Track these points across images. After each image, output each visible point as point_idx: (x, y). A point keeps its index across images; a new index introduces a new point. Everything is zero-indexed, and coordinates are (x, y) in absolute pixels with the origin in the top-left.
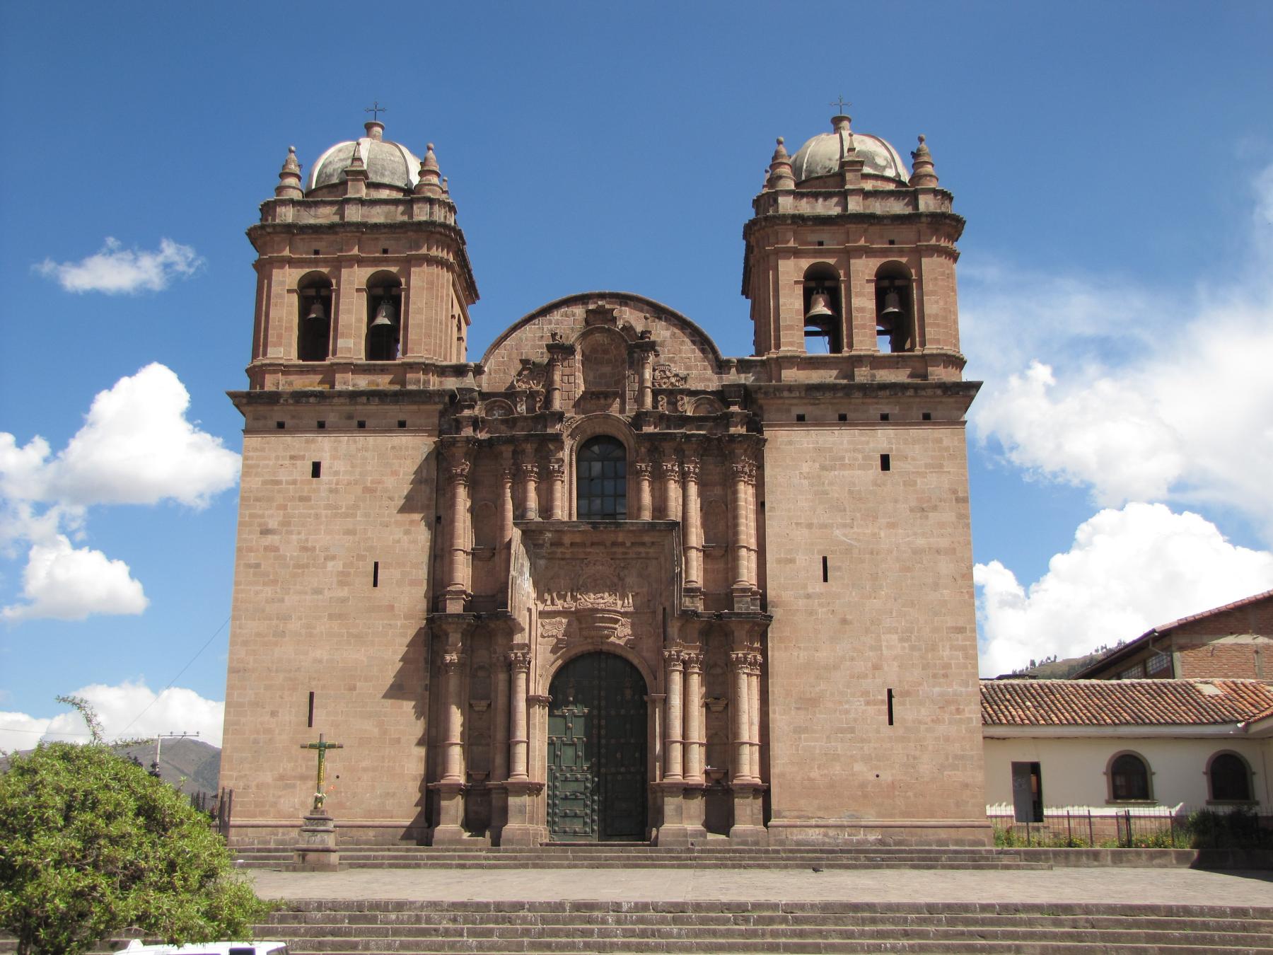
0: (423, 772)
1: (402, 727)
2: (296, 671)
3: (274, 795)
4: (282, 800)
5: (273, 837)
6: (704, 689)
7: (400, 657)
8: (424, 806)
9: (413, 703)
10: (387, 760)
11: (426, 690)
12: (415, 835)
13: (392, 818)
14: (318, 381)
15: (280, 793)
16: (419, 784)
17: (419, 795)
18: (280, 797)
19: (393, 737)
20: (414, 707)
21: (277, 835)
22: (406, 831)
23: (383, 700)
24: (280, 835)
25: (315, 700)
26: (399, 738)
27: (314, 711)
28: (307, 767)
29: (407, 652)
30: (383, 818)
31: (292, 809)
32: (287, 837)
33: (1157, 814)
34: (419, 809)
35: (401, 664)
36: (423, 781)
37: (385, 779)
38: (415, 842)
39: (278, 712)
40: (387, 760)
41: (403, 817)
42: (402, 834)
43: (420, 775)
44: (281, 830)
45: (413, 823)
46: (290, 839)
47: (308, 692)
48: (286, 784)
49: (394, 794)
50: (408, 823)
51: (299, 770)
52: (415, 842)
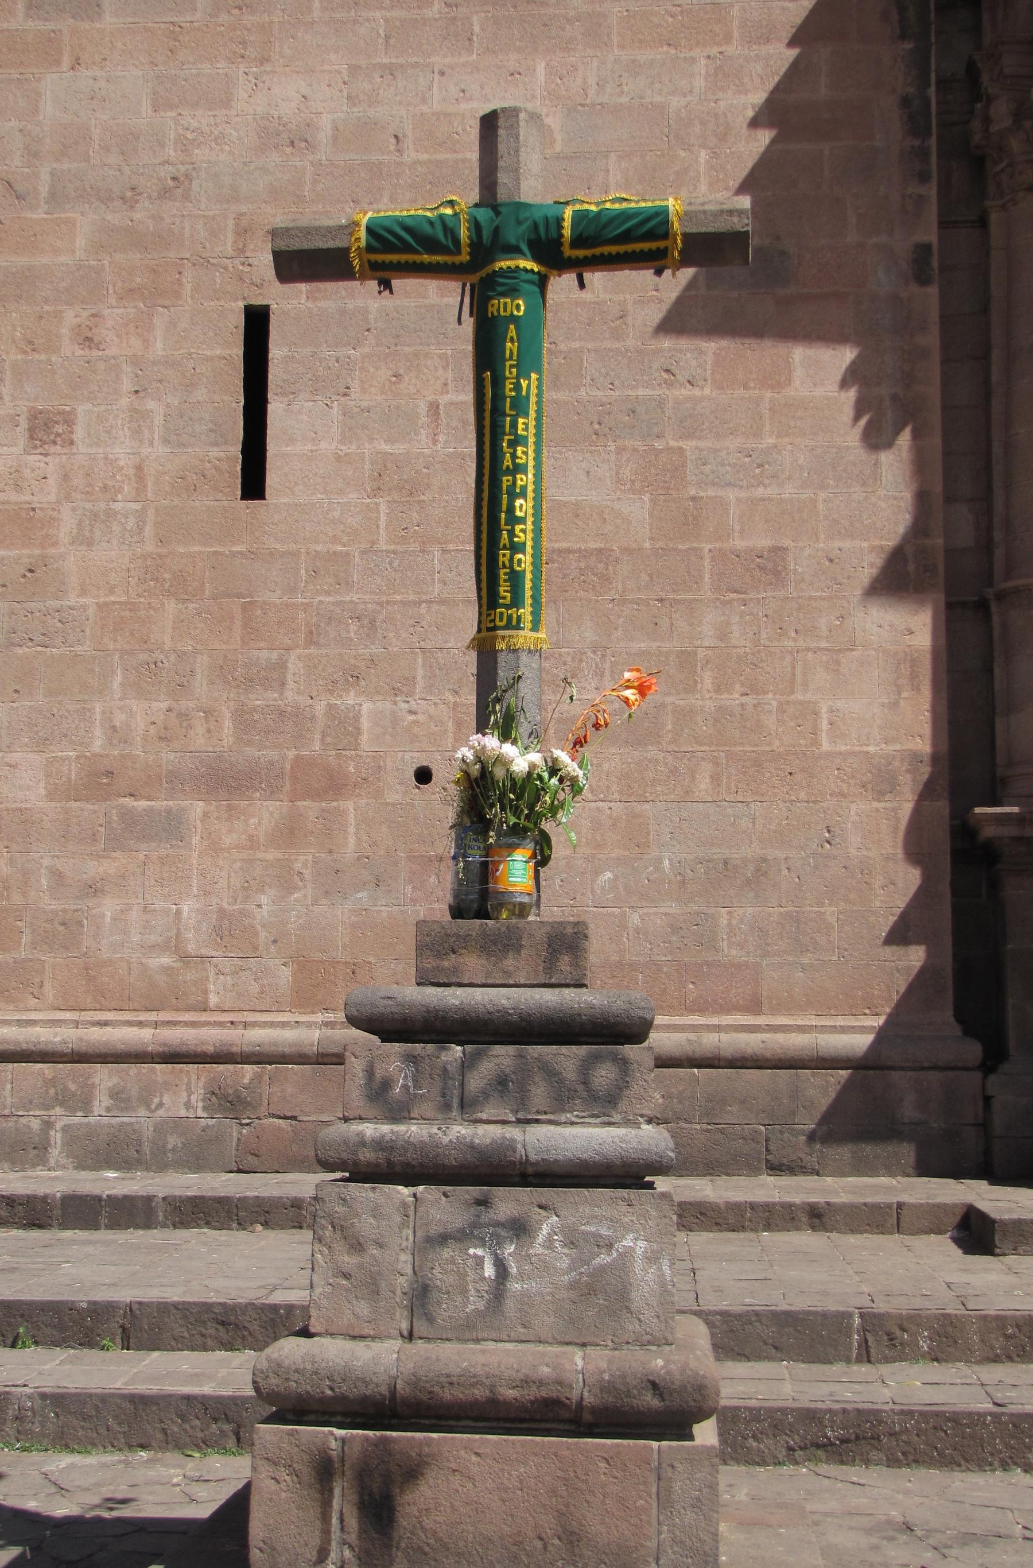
0: (923, 745)
1: (789, 491)
2: (165, 194)
3: (58, 877)
4: (108, 907)
5: (59, 1115)
6: (85, 1305)
7: (759, 97)
8: (947, 940)
9: (847, 355)
10: (707, 680)
11: (922, 278)
12: (908, 1111)
13: (754, 1006)
14: (655, 314)
15: (93, 869)
16: (907, 808)
17: (911, 878)
18: (94, 889)
19: (740, 544)
20: (851, 377)
21: (85, 1105)
22: (847, 1088)
23: (667, 343)
24: (101, 1102)
25: (276, 352)
26: (778, 551)
27: (276, 408)
28: (244, 720)
29: (794, 72)
30: (700, 1008)
31: (166, 960)
32: (141, 1119)
33: (459, 991)
34: (916, 956)
35: (765, 137)
36: (927, 792)
37: (703, 784)
38: (907, 1152)
39: (69, 420)
40: (707, 680)
41: (825, 1005)
42: (824, 1102)
43: (915, 758)
44: (104, 1076)
45: (882, 1036)
46: (161, 1129)
47: (241, 304)
48: (129, 818)
49: (762, 868)
50: (860, 1042)
51: (199, 739)
52: (907, 1152)
